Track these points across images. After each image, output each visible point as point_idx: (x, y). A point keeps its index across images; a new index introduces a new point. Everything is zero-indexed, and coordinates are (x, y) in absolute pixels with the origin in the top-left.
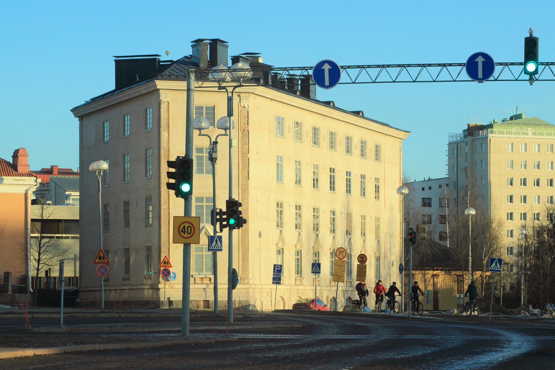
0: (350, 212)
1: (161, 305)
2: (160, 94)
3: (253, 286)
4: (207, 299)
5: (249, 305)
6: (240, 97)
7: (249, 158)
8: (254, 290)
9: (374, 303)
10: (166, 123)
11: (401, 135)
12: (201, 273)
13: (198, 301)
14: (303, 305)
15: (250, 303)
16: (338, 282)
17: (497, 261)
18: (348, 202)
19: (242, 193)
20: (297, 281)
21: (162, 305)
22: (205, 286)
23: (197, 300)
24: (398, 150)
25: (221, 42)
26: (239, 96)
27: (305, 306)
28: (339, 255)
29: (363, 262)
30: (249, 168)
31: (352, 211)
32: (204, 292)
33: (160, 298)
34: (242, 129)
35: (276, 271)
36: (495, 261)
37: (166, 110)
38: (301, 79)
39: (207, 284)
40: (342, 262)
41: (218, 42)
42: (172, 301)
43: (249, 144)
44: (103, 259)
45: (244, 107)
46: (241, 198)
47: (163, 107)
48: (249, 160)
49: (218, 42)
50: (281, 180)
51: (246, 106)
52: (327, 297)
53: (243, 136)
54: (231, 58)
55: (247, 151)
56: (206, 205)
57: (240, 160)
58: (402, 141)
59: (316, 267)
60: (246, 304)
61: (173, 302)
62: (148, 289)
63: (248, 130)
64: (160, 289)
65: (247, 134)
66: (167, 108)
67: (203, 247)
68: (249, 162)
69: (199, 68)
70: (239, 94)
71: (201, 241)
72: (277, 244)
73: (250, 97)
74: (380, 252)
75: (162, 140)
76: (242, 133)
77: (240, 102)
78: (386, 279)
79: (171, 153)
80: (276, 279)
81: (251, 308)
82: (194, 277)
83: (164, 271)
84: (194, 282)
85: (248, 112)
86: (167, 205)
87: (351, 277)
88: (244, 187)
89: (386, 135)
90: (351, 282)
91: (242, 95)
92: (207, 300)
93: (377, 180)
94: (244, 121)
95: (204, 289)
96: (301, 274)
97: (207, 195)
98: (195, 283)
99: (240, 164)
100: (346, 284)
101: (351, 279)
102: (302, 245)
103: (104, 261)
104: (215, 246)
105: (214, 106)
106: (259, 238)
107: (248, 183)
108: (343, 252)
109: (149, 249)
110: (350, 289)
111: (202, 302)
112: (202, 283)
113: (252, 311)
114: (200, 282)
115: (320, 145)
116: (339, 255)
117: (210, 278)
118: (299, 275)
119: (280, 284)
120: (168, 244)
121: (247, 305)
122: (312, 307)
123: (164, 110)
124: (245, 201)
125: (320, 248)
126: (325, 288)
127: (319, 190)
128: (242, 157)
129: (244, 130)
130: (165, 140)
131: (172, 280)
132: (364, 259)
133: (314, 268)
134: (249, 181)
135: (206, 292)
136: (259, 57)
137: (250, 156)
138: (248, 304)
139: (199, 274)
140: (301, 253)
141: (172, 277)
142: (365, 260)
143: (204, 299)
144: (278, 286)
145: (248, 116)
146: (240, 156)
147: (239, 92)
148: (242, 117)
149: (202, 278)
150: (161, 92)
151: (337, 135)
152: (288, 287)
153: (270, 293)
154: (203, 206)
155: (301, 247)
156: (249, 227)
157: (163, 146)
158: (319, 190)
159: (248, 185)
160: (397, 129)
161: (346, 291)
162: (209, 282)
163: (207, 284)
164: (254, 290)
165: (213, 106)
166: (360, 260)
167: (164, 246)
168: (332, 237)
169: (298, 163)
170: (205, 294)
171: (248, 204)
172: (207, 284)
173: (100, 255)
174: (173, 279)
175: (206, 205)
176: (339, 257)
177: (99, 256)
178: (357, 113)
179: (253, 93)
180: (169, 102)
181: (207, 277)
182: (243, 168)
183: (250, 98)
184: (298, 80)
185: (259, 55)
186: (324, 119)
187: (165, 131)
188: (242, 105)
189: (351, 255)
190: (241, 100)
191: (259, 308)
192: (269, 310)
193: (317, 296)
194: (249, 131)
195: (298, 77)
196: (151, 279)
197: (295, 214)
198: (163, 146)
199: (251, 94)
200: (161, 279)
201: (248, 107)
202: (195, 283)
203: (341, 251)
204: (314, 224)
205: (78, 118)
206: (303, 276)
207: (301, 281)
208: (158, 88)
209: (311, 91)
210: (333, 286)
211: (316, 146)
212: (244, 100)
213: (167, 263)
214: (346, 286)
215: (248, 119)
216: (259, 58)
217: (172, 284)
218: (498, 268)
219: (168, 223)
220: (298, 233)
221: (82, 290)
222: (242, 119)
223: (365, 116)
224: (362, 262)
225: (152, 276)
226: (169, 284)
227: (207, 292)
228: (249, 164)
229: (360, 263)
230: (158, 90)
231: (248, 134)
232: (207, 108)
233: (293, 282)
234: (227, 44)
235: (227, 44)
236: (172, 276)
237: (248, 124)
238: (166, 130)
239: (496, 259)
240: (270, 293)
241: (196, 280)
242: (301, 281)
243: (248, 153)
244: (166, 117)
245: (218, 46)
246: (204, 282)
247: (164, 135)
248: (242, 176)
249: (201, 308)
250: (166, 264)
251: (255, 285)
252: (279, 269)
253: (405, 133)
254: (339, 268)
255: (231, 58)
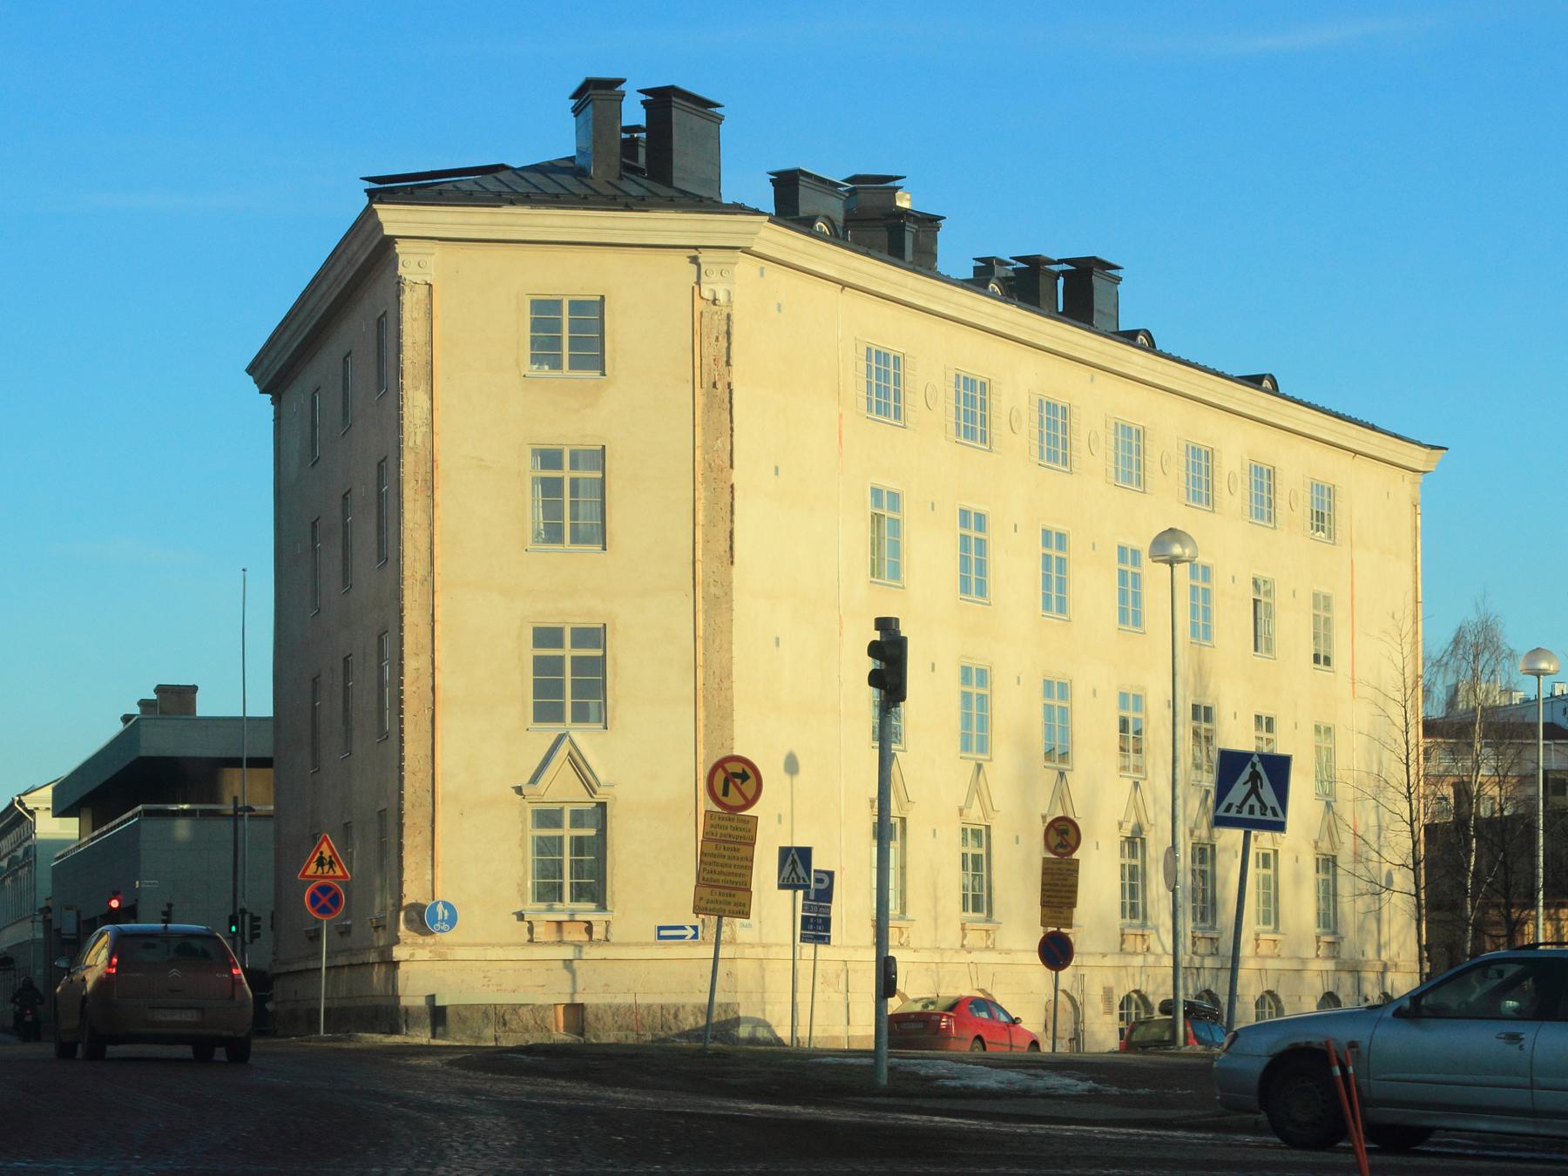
0: (1208, 702)
1: (402, 1022)
2: (397, 255)
3: (760, 952)
4: (578, 1000)
5: (737, 1021)
6: (699, 266)
7: (732, 486)
8: (761, 965)
9: (1254, 1007)
10: (422, 360)
11: (1417, 457)
12: (557, 905)
13: (540, 1006)
14: (913, 1021)
15: (742, 1014)
16: (720, 918)
17: (1260, 768)
18: (1200, 669)
19: (706, 612)
20: (970, 935)
21: (406, 1021)
22: (568, 952)
23: (538, 1002)
24: (1408, 510)
25: (687, 100)
26: (694, 260)
27: (921, 1026)
28: (726, 793)
29: (1065, 847)
30: (732, 521)
31: (1217, 699)
32: (566, 975)
33: (398, 997)
34: (705, 380)
35: (812, 896)
36: (1248, 770)
37: (420, 313)
38: (1064, 273)
39: (578, 946)
40: (740, 825)
41: (674, 99)
42: (443, 1008)
43: (732, 436)
44: (331, 867)
45: (714, 302)
46: (705, 631)
47: (411, 302)
48: (732, 492)
49: (674, 99)
50: (896, 573)
51: (722, 297)
52: (1108, 994)
53: (708, 407)
54: (771, 180)
55: (726, 458)
56: (573, 658)
57: (700, 494)
58: (1420, 477)
59: (794, 862)
60: (724, 1018)
61: (448, 1011)
62: (379, 963)
63: (729, 384)
64: (398, 962)
65: (727, 400)
66: (423, 306)
67: (561, 810)
68: (733, 498)
69: (585, 180)
70: (693, 253)
71: (268, 756)
72: (961, 811)
73: (736, 264)
74: (1336, 839)
75: (406, 422)
76: (708, 395)
77: (698, 283)
78: (1361, 928)
79: (440, 468)
80: (815, 924)
81: (744, 1032)
82: (527, 918)
83: (319, 894)
84: (527, 937)
85: (729, 316)
86: (426, 658)
87: (1214, 922)
88: (713, 590)
89: (1356, 453)
90: (1212, 939)
91: (704, 257)
92: (579, 1004)
93: (1322, 603)
94: (712, 349)
95: (568, 964)
96: (1145, 917)
97: (578, 620)
98: (531, 941)
99: (700, 506)
100: (1194, 944)
101: (1213, 928)
102: (989, 808)
103: (331, 873)
104: (1240, 808)
105: (603, 297)
106: (786, 778)
107: (729, 575)
108: (744, 777)
109: (382, 814)
110: (1209, 962)
111: (560, 1009)
112: (561, 942)
113: (753, 1040)
114: (554, 938)
115: (1075, 464)
116: (726, 793)
117: (589, 922)
118: (983, 915)
119: (829, 943)
120: (430, 799)
121: (727, 1021)
122: (948, 1027)
123: (415, 315)
124: (718, 640)
125: (992, 815)
126: (1098, 961)
127: (1069, 621)
128: (706, 480)
129: (714, 385)
130: (418, 422)
131: (441, 931)
132: (1071, 839)
133: (788, 868)
134: (736, 569)
135: (573, 973)
136: (897, 189)
137: (737, 477)
138: (731, 1015)
139: (550, 909)
140: (989, 836)
141: (443, 920)
142: (1073, 843)
143: (567, 1000)
144: (821, 948)
145: (728, 333)
146: (699, 478)
147: (696, 248)
148: (705, 338)
149: (559, 923)
150: (400, 247)
151: (1147, 436)
152: (924, 956)
153: (838, 976)
154: (561, 658)
155: (986, 817)
156: (736, 735)
157: (411, 444)
158: (1069, 621)
159: (731, 583)
160: (1396, 436)
161: (1195, 971)
162: (585, 937)
163: (576, 946)
164: (761, 965)
165: (598, 298)
166: (1055, 840)
167: (413, 806)
168: (1129, 783)
169: (973, 520)
170: (569, 983)
171: (730, 650)
172: (578, 946)
173: (322, 853)
174: (445, 926)
175: (573, 658)
176: (724, 799)
177: (318, 855)
178: (1254, 381)
179: (746, 251)
180: (430, 285)
181: (578, 917)
182: (711, 523)
183: (737, 266)
184: (1057, 276)
185: (897, 183)
186: (1092, 380)
187: (416, 388)
188: (707, 294)
189: (1213, 847)
190: (703, 276)
191: (784, 1033)
192: (837, 1038)
193: (1060, 987)
194: (734, 386)
195: (1055, 268)
196: (384, 927)
197: (956, 701)
198: (411, 444)
199: (738, 253)
200: (402, 926)
201: (729, 300)
202: (531, 941)
203: (736, 775)
204: (1138, 751)
205: (270, 396)
206: (995, 917)
207: (988, 936)
208: (387, 232)
209: (1100, 312)
210: (1135, 953)
211: (1055, 466)
212: (715, 277)
213: (331, 864)
214: (1194, 953)
215: (729, 344)
216: (899, 193)
217: (443, 944)
218: (799, 878)
219: (429, 724)
220: (973, 764)
221: (284, 969)
222: (705, 345)
223: (1281, 391)
224: (1060, 850)
225: (388, 918)
226: (435, 944)
227: (579, 974)
228: (732, 506)
229: (1055, 854)
230: (390, 241)
231: (731, 398)
232: (576, 306)
233: (952, 936)
234: (718, 110)
235: (718, 110)
236: (440, 917)
237: (728, 363)
238: (423, 387)
239: (1255, 759)
240: (838, 976)
241: (535, 930)
242: (988, 936)
243: (732, 467)
244: (421, 337)
245: (675, 112)
246: (567, 938)
247: (414, 403)
248: (705, 550)
249: (560, 1035)
250: (326, 868)
251: (764, 946)
252: (822, 886)
253: (1428, 451)
254: (727, 853)
255: (771, 180)
